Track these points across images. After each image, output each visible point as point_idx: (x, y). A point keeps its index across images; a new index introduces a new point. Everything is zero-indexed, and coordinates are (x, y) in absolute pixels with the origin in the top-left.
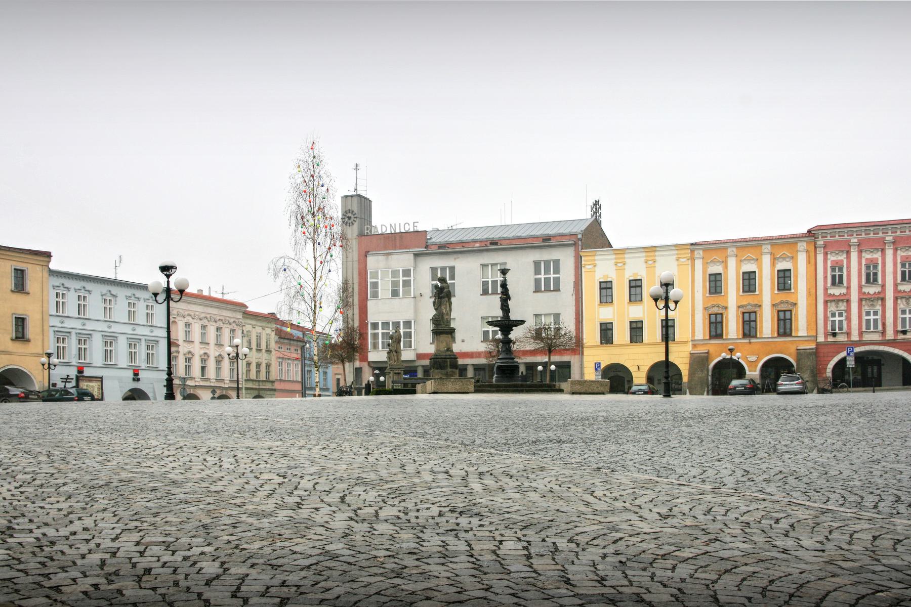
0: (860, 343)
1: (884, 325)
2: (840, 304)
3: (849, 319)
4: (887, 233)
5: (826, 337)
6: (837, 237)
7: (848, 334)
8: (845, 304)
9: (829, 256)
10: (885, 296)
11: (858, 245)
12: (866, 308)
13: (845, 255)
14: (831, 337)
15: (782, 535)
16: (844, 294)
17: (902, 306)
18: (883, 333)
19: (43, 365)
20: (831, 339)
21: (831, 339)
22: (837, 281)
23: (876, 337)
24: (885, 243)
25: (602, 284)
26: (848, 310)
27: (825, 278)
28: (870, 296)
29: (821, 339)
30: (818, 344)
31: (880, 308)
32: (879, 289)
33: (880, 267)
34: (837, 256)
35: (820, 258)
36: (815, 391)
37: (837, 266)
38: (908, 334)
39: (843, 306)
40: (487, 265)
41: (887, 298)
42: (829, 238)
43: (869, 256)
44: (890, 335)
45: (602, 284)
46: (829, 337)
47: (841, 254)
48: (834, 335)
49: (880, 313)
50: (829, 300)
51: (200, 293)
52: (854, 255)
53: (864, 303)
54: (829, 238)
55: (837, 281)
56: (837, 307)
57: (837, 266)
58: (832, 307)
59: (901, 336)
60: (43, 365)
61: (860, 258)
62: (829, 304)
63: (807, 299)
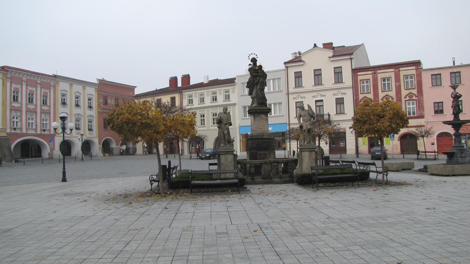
0: (26, 135)
1: (36, 125)
2: (18, 112)
3: (21, 121)
4: (24, 76)
5: (11, 130)
6: (17, 75)
7: (21, 129)
8: (20, 112)
9: (13, 84)
10: (37, 111)
11: (11, 79)
12: (29, 116)
13: (20, 86)
14: (43, 131)
15: (406, 220)
16: (19, 107)
17: (43, 117)
18: (36, 130)
19: (79, 139)
20: (13, 131)
21: (13, 131)
22: (15, 99)
23: (33, 132)
24: (51, 86)
25: (297, 103)
26: (21, 116)
27: (11, 96)
28: (30, 110)
29: (8, 131)
30: (7, 134)
31: (49, 118)
32: (34, 107)
33: (48, 97)
34: (32, 88)
35: (8, 84)
36: (14, 161)
37: (16, 91)
38: (46, 131)
39: (19, 114)
40: (275, 79)
41: (38, 112)
42: (13, 74)
43: (30, 89)
44: (39, 132)
45: (297, 103)
46: (12, 130)
47: (18, 84)
48: (15, 129)
49: (35, 119)
50: (13, 109)
51: (461, 64)
52: (24, 87)
53: (28, 113)
54: (13, 74)
55: (15, 99)
56: (16, 114)
57: (16, 91)
58: (14, 114)
59: (43, 132)
60: (79, 139)
61: (27, 89)
62: (12, 111)
63: (2, 107)
